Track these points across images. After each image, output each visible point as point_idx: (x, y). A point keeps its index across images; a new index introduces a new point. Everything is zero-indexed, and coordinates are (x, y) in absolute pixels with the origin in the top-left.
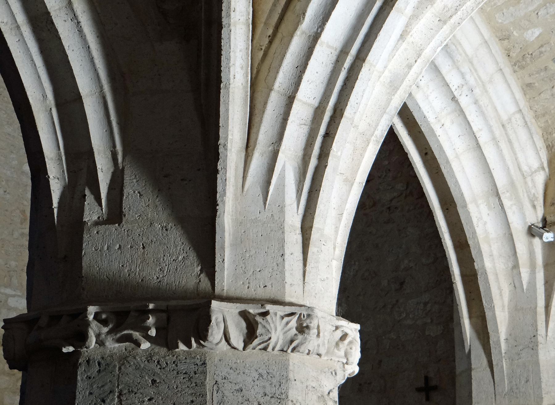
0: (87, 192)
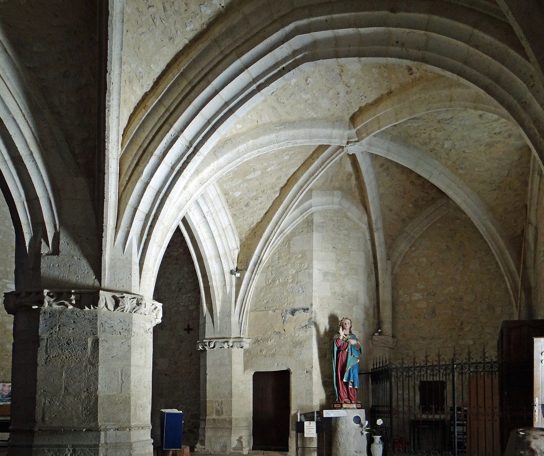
0: (42, 240)
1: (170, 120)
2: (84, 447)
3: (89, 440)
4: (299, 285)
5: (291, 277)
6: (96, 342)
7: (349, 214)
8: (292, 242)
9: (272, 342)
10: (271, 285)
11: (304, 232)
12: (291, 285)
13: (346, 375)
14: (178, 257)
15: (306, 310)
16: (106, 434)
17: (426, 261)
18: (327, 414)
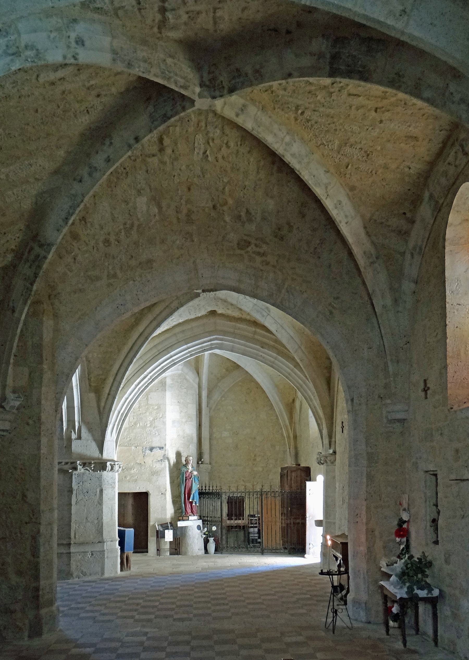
0: (72, 431)
1: (145, 367)
2: (97, 552)
3: (97, 548)
4: (155, 429)
5: (149, 422)
6: (101, 491)
7: (187, 377)
8: (149, 396)
9: (134, 470)
10: (133, 427)
11: (159, 390)
12: (149, 429)
13: (192, 496)
15: (161, 448)
16: (106, 544)
17: (231, 409)
18: (180, 524)
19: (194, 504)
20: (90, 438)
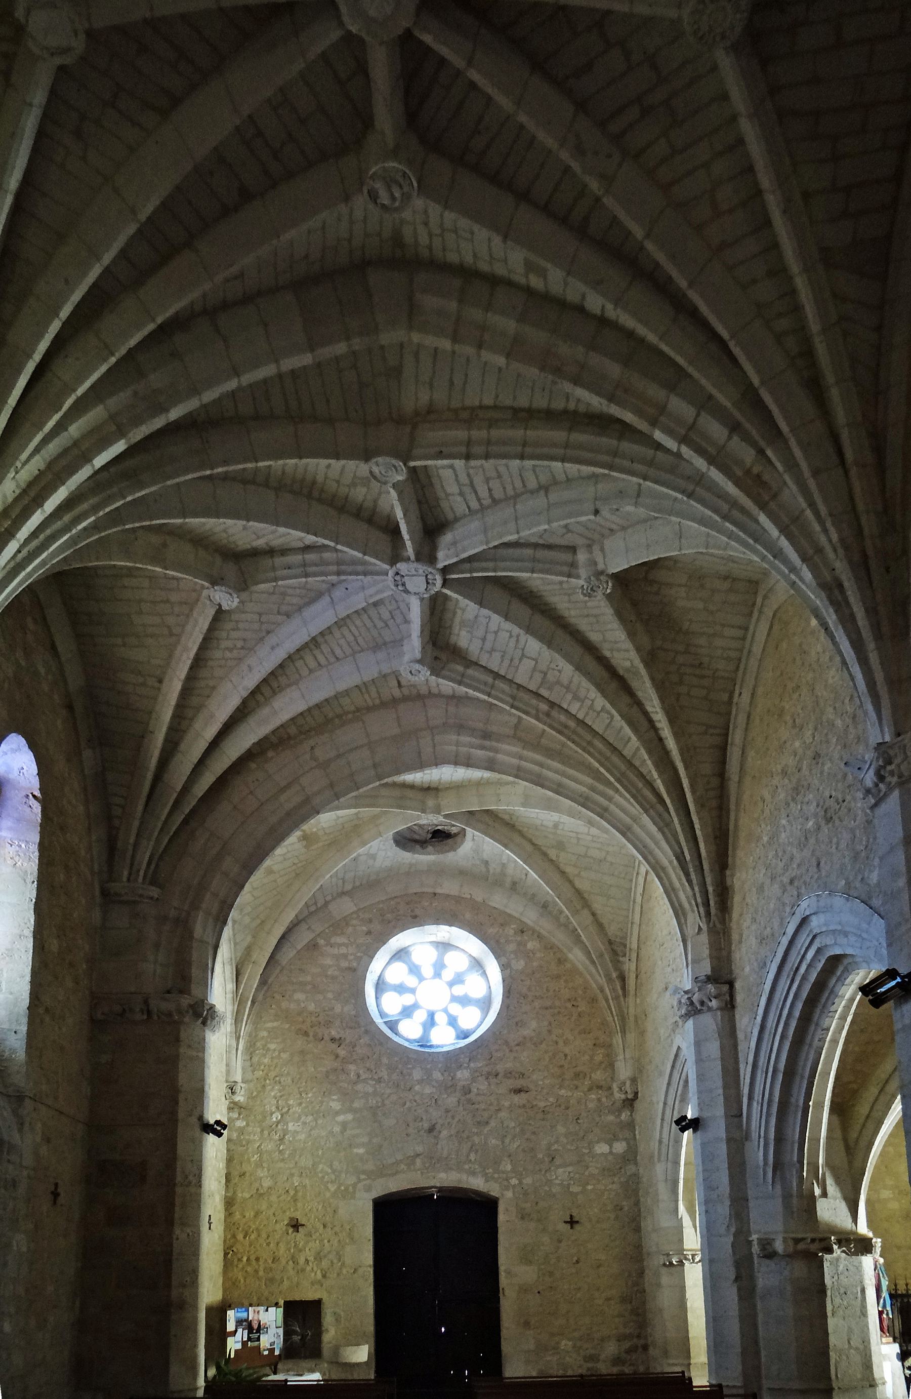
14: (547, 1109)
19: (885, 1316)
20: (839, 1195)
